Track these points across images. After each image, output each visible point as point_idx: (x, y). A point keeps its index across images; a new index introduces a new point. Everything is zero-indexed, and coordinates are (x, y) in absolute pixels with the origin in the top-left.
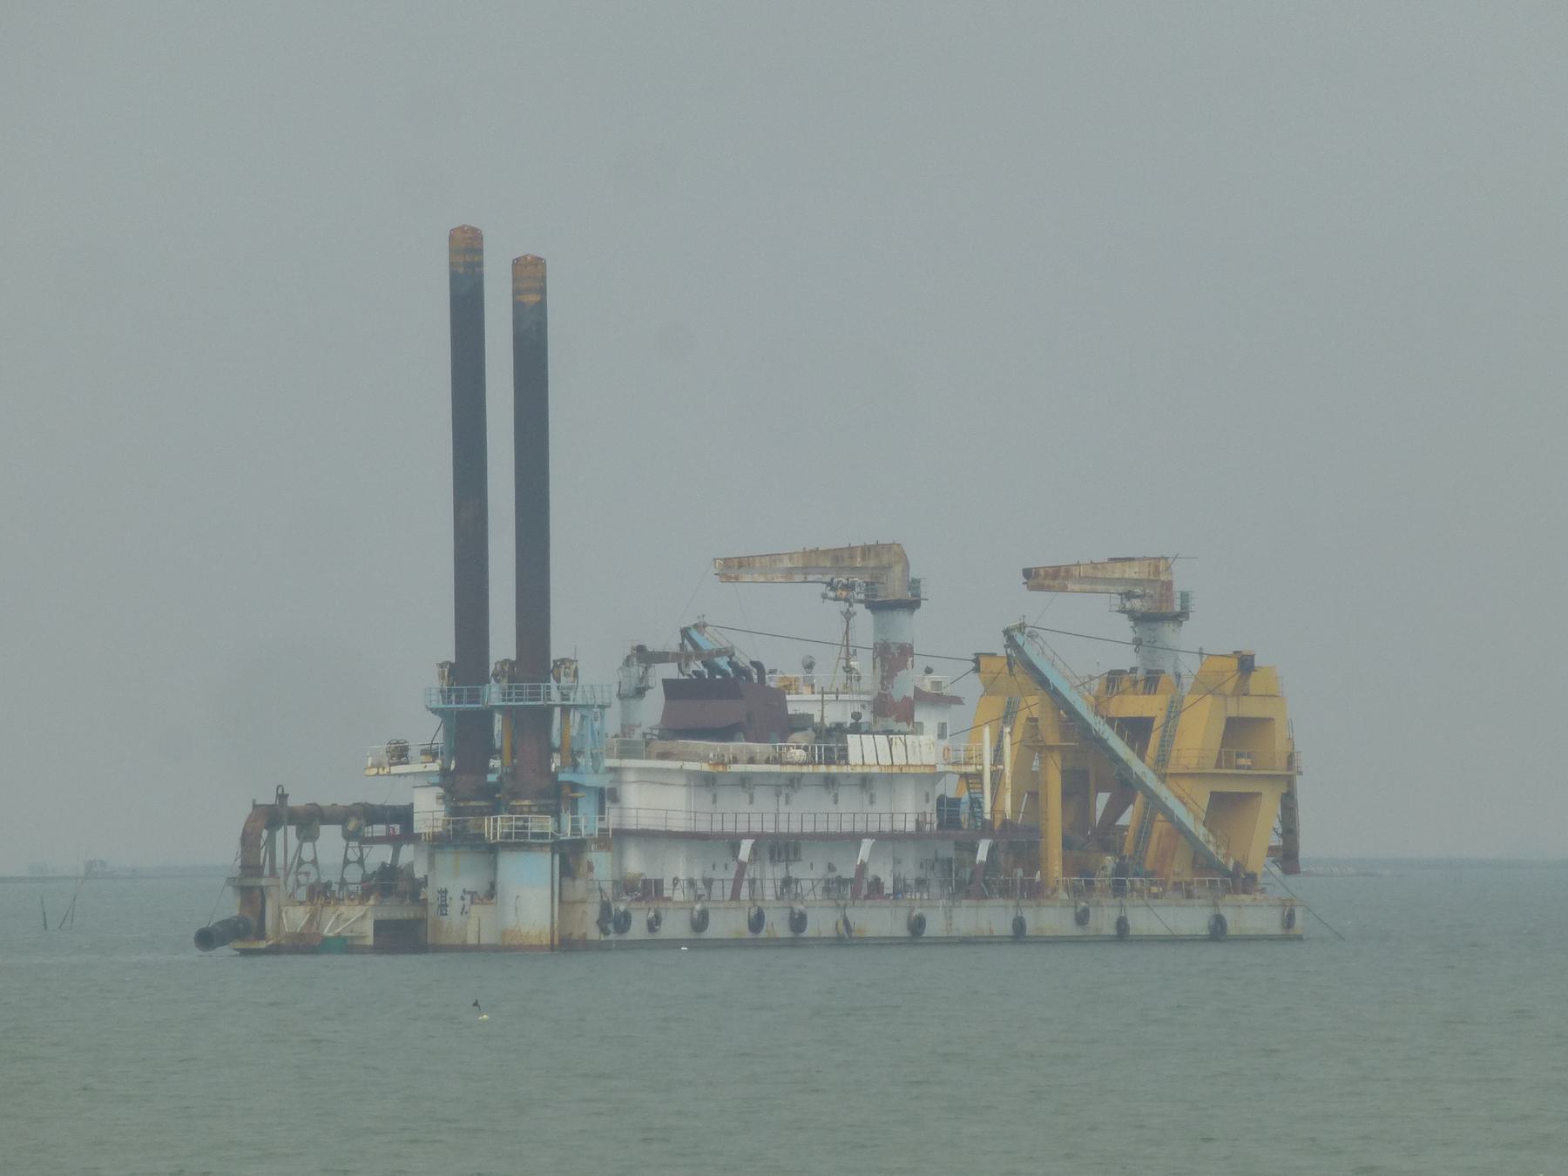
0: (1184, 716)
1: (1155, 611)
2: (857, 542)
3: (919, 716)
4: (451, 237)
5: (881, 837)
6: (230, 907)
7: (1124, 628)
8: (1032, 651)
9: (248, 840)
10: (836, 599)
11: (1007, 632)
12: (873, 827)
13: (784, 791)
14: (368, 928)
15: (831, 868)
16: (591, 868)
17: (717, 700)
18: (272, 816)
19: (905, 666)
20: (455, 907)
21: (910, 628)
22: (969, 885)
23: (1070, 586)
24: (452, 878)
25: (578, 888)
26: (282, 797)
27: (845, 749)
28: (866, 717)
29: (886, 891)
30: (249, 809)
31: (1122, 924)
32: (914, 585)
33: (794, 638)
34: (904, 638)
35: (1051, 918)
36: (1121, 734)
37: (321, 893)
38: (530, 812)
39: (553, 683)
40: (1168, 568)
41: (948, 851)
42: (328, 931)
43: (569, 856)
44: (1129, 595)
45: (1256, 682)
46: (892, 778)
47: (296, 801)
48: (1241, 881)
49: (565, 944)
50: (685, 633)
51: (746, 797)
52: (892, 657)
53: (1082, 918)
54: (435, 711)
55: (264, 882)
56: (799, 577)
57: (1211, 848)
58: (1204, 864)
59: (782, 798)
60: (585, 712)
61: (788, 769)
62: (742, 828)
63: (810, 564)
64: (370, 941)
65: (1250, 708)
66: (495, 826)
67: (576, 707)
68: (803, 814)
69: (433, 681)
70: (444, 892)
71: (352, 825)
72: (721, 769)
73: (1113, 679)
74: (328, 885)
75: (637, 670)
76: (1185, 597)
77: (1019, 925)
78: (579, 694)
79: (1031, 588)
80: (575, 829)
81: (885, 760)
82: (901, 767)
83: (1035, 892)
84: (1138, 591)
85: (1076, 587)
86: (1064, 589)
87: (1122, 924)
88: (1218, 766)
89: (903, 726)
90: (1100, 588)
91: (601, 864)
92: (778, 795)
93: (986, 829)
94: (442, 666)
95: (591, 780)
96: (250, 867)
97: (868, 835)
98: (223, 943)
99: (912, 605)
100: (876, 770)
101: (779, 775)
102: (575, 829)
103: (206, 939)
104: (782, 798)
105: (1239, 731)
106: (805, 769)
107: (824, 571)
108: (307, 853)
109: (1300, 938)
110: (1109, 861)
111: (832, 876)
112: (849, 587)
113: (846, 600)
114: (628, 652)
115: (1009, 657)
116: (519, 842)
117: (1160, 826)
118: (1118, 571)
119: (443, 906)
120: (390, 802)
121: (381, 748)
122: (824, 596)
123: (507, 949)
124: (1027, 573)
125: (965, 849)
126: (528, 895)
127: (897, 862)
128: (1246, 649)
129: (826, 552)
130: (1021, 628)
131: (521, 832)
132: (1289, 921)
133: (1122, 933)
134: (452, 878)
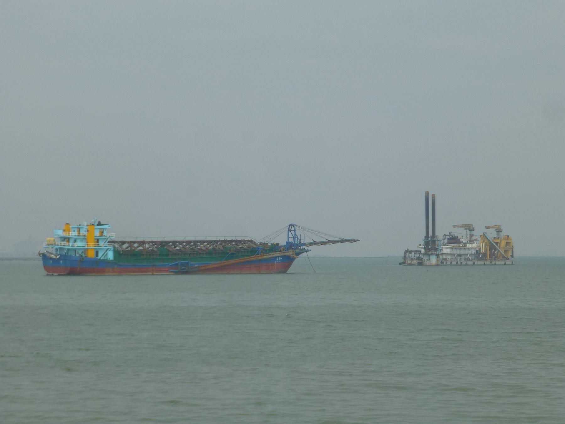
1: (499, 231)
6: (403, 261)
7: (496, 233)
9: (404, 254)
17: (453, 240)
18: (407, 251)
21: (473, 233)
22: (479, 259)
24: (425, 258)
33: (461, 233)
35: (488, 263)
37: (412, 259)
43: (438, 256)
46: (471, 248)
48: (507, 259)
49: (437, 265)
52: (471, 236)
58: (504, 257)
65: (509, 241)
66: (430, 253)
73: (494, 238)
83: (486, 260)
91: (441, 257)
93: (481, 253)
96: (405, 256)
99: (473, 230)
103: (400, 264)
105: (508, 243)
116: (432, 254)
123: (431, 265)
125: (479, 256)
126: (433, 260)
133: (495, 264)
134: (425, 258)
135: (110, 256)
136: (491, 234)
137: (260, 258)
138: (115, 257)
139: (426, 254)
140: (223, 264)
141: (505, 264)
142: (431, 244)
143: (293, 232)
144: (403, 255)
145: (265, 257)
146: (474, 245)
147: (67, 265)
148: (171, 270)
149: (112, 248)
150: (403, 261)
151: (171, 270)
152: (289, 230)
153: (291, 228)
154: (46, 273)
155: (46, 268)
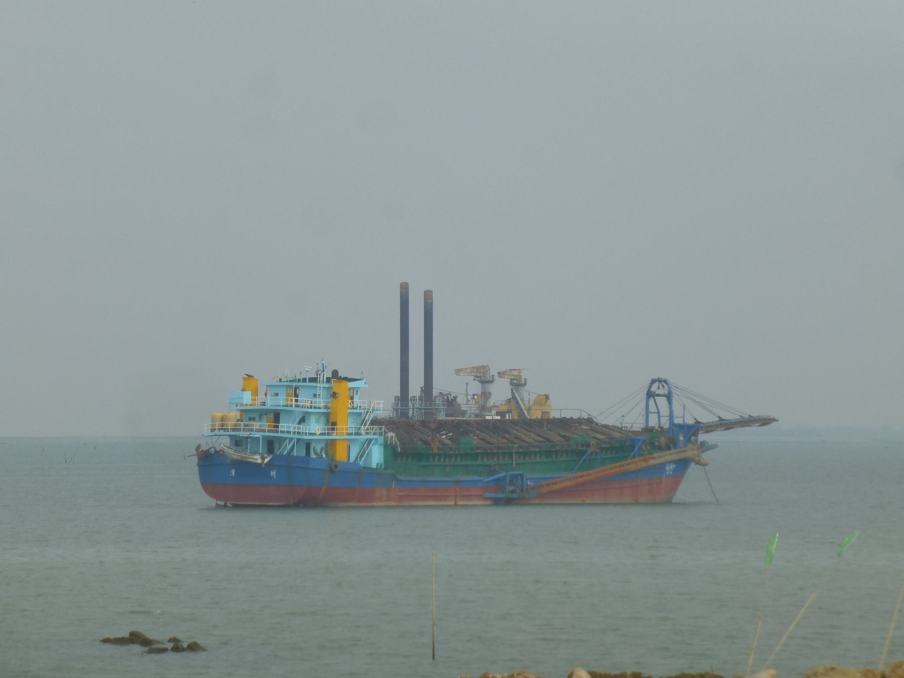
1: (517, 384)
135: (377, 457)
137: (643, 464)
138: (385, 461)
140: (580, 480)
143: (662, 402)
145: (652, 462)
147: (260, 475)
148: (487, 495)
149: (381, 439)
151: (487, 495)
152: (650, 395)
153: (658, 389)
154: (212, 502)
155: (210, 484)
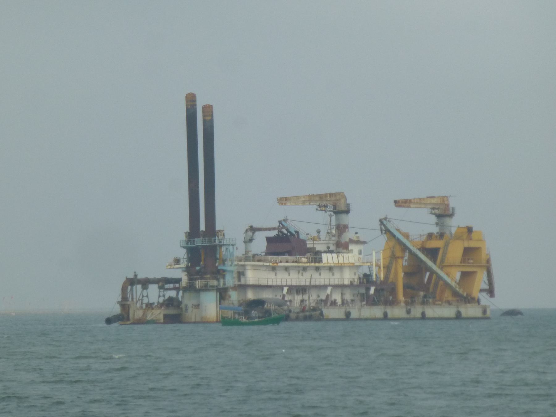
0: (383, 249)
1: (443, 213)
2: (328, 192)
3: (351, 247)
4: (186, 97)
5: (335, 287)
6: (117, 310)
7: (434, 219)
8: (390, 226)
9: (124, 289)
10: (321, 210)
11: (381, 221)
12: (332, 283)
13: (301, 272)
14: (161, 317)
15: (319, 296)
16: (230, 297)
17: (285, 243)
18: (132, 282)
19: (345, 231)
20: (190, 309)
21: (347, 219)
22: (372, 302)
23: (412, 206)
24: (188, 300)
25: (226, 303)
26: (136, 276)
27: (321, 258)
28: (332, 248)
29: (339, 304)
30: (125, 279)
31: (423, 314)
32: (348, 205)
33: (310, 223)
34: (346, 223)
35: (398, 311)
36: (423, 253)
37: (150, 306)
38: (210, 279)
39: (217, 238)
40: (447, 200)
41: (363, 291)
42: (148, 318)
43: (222, 293)
44: (433, 209)
45: (474, 236)
46: (341, 267)
47: (141, 276)
48: (469, 300)
49: (225, 321)
50: (280, 222)
51: (274, 274)
52: (341, 229)
53: (408, 312)
54: (184, 247)
55: (128, 303)
56: (307, 203)
57: (458, 289)
58: (455, 294)
59: (300, 274)
60: (227, 247)
61: (300, 264)
62: (284, 284)
63: (311, 199)
64: (162, 321)
65: (472, 244)
66: (198, 284)
67: (224, 245)
68: (304, 279)
69: (183, 237)
70: (186, 305)
71: (160, 284)
72: (276, 265)
73: (430, 236)
74: (152, 304)
75: (250, 234)
76: (453, 209)
77: (385, 314)
78: (225, 241)
79: (397, 206)
80: (224, 284)
81: (336, 261)
82: (341, 264)
83: (393, 303)
84: (436, 207)
85: (414, 206)
86: (409, 207)
87: (423, 314)
88: (461, 262)
89: (345, 251)
90: (423, 206)
91: (234, 296)
92: (299, 273)
93: (373, 283)
94: (186, 233)
95: (234, 269)
96: (124, 298)
97: (330, 285)
98: (115, 322)
99: (347, 212)
100: (332, 265)
101: (299, 267)
102: (224, 284)
103: (109, 321)
104: (300, 274)
105: (468, 251)
106: (307, 265)
107: (316, 201)
108: (145, 294)
109: (488, 318)
110: (422, 294)
111: (318, 299)
112: (325, 206)
113: (325, 211)
114: (248, 228)
115: (381, 228)
116: (206, 289)
117: (441, 282)
118: (429, 201)
119: (186, 309)
120: (174, 277)
121: (171, 260)
122: (317, 209)
123: (204, 322)
124: (395, 202)
125: (374, 291)
126: (210, 306)
127: (342, 294)
128: (470, 225)
129: (316, 195)
130: (385, 219)
131: (206, 285)
132: (484, 312)
133: (423, 316)
134: (188, 300)
136: (418, 225)
139: (190, 288)
141: (458, 316)
142: (204, 253)
144: (117, 296)
146: (352, 256)
150: (117, 310)
